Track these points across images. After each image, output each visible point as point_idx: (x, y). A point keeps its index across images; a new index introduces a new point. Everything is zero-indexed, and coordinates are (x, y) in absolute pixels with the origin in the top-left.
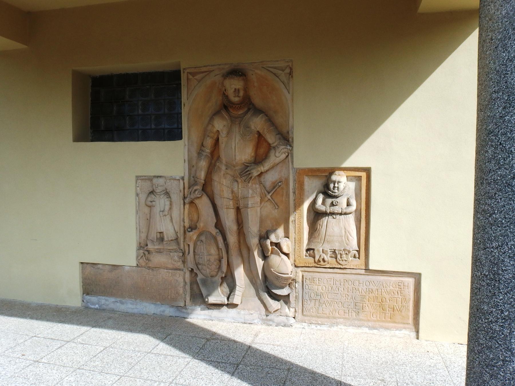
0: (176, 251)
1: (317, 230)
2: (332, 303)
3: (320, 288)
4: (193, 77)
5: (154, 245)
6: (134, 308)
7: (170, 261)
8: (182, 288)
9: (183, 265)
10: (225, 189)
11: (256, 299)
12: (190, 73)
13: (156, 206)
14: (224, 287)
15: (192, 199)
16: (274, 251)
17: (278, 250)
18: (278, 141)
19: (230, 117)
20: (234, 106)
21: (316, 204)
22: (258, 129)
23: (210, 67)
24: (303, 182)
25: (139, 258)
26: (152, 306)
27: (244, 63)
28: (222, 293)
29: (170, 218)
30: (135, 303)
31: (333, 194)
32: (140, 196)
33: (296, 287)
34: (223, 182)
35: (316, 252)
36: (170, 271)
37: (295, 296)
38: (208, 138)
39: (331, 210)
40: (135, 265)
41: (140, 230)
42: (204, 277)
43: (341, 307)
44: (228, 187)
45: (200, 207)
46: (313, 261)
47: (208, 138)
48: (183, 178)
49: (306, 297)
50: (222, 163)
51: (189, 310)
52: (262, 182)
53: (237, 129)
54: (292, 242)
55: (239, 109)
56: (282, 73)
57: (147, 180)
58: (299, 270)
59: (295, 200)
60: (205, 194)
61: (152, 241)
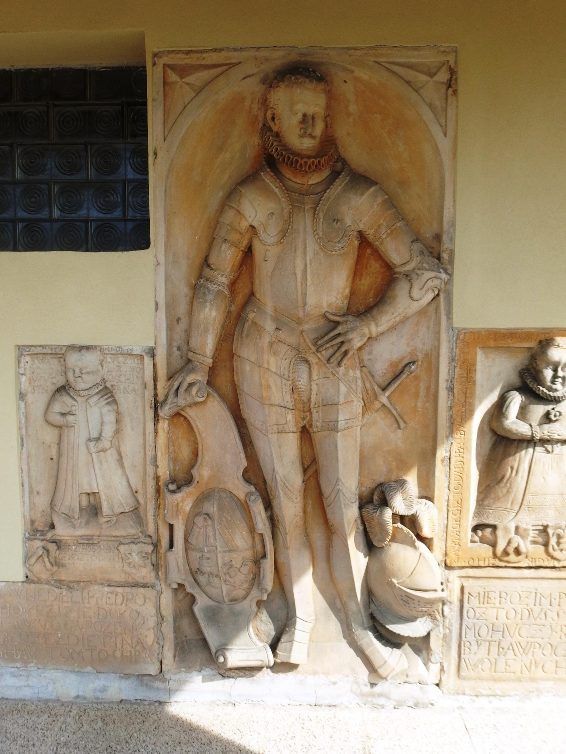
0: (136, 541)
1: (505, 480)
2: (529, 646)
3: (502, 613)
4: (182, 77)
5: (74, 527)
6: (20, 687)
7: (118, 565)
8: (152, 631)
9: (153, 574)
10: (274, 382)
11: (344, 645)
12: (172, 67)
13: (76, 426)
14: (261, 621)
15: (179, 408)
16: (399, 536)
17: (411, 533)
18: (419, 258)
19: (288, 190)
20: (302, 161)
21: (507, 418)
22: (361, 227)
23: (231, 54)
24: (474, 365)
25: (33, 560)
26: (73, 678)
27: (326, 49)
28: (257, 635)
29: (116, 456)
30: (24, 673)
31: (551, 394)
32: (30, 398)
33: (445, 614)
34: (268, 363)
35: (499, 533)
36: (120, 590)
37: (441, 636)
38: (223, 248)
39: (546, 433)
40: (22, 578)
41: (31, 487)
42: (211, 603)
43: (551, 654)
44: (282, 377)
45: (199, 426)
46: (491, 554)
47: (225, 247)
48: (152, 353)
49: (469, 636)
50: (265, 313)
51: (171, 682)
52: (366, 363)
53: (309, 222)
54: (440, 510)
55: (314, 171)
56: (427, 82)
57: (49, 357)
58: (454, 575)
59: (451, 408)
60: (215, 395)
61: (68, 518)
